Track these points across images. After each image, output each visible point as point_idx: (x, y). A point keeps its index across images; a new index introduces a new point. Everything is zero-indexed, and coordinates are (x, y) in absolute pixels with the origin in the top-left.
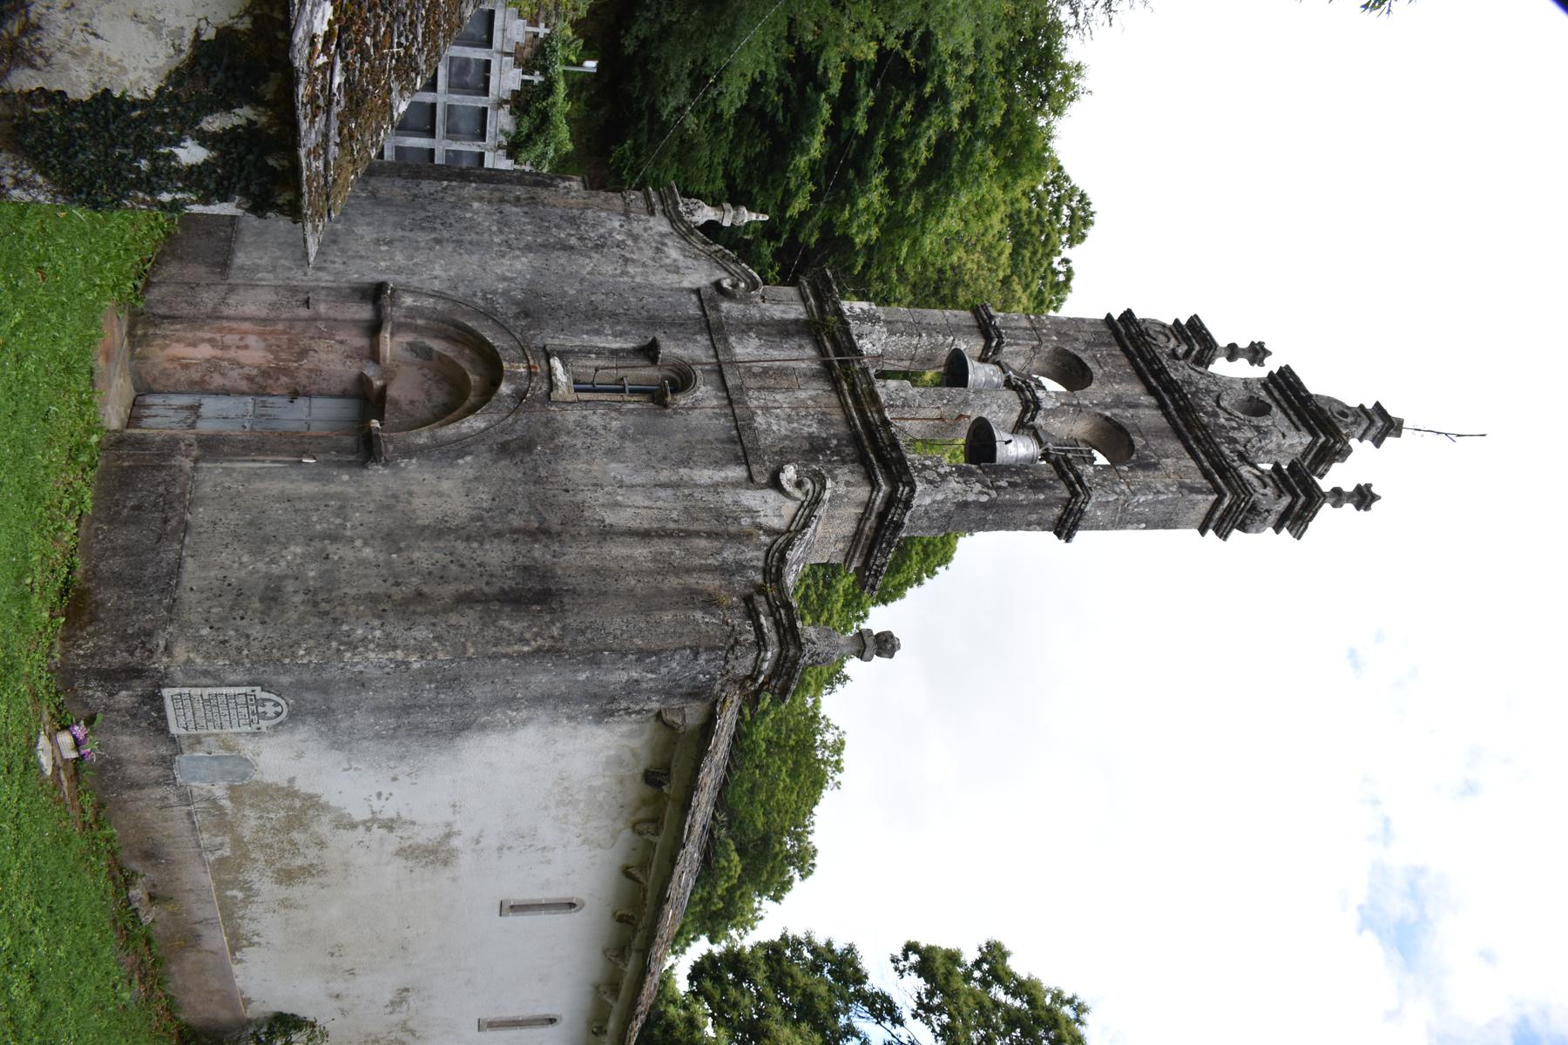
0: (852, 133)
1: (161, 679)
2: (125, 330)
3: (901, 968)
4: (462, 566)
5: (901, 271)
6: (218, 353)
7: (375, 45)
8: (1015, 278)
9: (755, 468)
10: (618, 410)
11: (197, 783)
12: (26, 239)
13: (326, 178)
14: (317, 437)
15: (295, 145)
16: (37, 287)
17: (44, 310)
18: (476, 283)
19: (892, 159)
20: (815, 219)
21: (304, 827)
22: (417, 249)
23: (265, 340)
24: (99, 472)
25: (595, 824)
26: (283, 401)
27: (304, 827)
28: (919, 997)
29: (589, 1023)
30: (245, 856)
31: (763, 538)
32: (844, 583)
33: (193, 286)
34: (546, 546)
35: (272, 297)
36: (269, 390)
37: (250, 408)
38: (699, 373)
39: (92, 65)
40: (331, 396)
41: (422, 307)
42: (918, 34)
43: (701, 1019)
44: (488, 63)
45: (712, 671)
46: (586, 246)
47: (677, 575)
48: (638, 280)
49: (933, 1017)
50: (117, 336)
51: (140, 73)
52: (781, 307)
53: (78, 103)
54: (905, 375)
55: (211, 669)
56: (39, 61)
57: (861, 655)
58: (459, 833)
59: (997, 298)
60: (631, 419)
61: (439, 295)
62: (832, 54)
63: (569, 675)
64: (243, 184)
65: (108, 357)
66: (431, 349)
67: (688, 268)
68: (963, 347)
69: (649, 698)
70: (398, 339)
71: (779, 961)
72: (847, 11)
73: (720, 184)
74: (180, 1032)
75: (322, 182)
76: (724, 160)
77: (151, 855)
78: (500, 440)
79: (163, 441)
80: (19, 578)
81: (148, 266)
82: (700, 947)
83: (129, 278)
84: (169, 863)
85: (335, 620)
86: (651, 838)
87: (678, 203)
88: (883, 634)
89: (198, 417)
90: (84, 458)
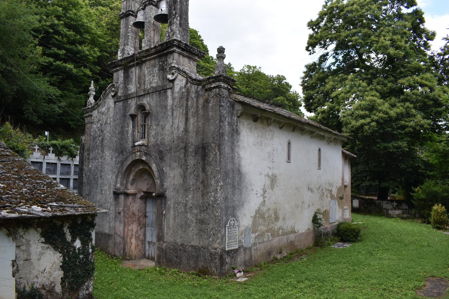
0: (65, 55)
1: (223, 251)
2: (127, 262)
3: (313, 52)
4: (194, 171)
5: (108, 41)
6: (134, 237)
7: (44, 194)
8: (110, 6)
9: (168, 87)
10: (150, 126)
11: (251, 241)
12: (103, 287)
13: (84, 207)
14: (158, 210)
15: (74, 215)
16: (116, 284)
17: (123, 282)
18: (113, 166)
19: (73, 43)
20: (92, 67)
21: (264, 214)
22: (103, 183)
23: (130, 224)
24: (167, 267)
25: (267, 136)
26: (147, 219)
27: (264, 214)
28: (321, 47)
29: (321, 140)
30: (271, 229)
31: (189, 85)
32: (202, 63)
33: (115, 244)
34: (189, 147)
35: (118, 223)
36: (144, 223)
37: (149, 228)
38: (139, 103)
39: (53, 271)
40: (146, 206)
41: (120, 181)
42: (33, 33)
43: (322, 110)
44: (47, 163)
45: (226, 101)
46: (102, 135)
47: (199, 111)
48: (112, 120)
49: (327, 44)
50: (129, 264)
51: (55, 258)
52: (120, 77)
53: (64, 274)
54: (141, 41)
55: (221, 238)
56: (53, 285)
57: (224, 58)
58: (268, 173)
59: (116, 12)
60: (153, 122)
61: (117, 177)
62: (41, 60)
63: (226, 142)
64: (86, 230)
65: (135, 266)
66: (133, 179)
67: (108, 105)
68: (132, 23)
69: (233, 120)
70: (130, 188)
71: (308, 87)
72: (27, 55)
73: (82, 96)
74: (315, 246)
75: (85, 208)
76: (75, 94)
77: (269, 253)
78: (159, 160)
79: (158, 251)
80: (195, 287)
81: (109, 256)
82: (303, 109)
83: (113, 261)
84: (272, 248)
85: (208, 205)
86: (272, 120)
87: (88, 108)
88: (218, 51)
89: (152, 242)
90: (163, 271)
